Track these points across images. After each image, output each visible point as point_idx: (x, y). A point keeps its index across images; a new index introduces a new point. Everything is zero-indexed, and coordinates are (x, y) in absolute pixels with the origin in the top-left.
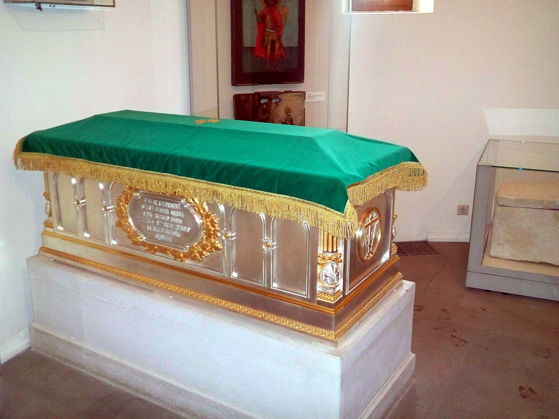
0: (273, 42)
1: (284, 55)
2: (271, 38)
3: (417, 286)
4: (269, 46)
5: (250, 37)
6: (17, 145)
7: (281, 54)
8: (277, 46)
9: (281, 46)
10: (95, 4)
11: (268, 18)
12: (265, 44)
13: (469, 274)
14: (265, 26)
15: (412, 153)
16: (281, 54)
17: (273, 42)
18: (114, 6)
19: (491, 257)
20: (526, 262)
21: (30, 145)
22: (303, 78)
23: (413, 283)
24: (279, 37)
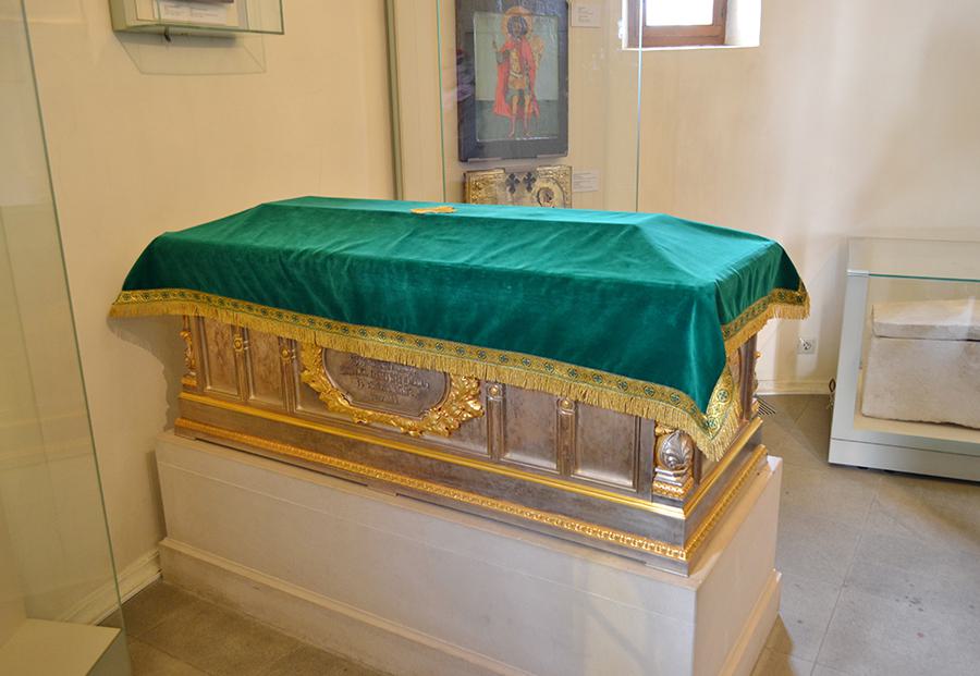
0: (521, 93)
1: (537, 113)
2: (518, 87)
3: (784, 462)
4: (515, 100)
5: (544, 39)
6: (123, 337)
7: (534, 112)
8: (527, 98)
9: (533, 99)
10: (251, 28)
11: (514, 55)
12: (509, 97)
13: (832, 441)
14: (509, 67)
15: (784, 252)
16: (534, 112)
17: (521, 93)
18: (282, 33)
19: (863, 415)
20: (921, 422)
21: (160, 267)
22: (567, 148)
23: (779, 460)
24: (530, 86)
